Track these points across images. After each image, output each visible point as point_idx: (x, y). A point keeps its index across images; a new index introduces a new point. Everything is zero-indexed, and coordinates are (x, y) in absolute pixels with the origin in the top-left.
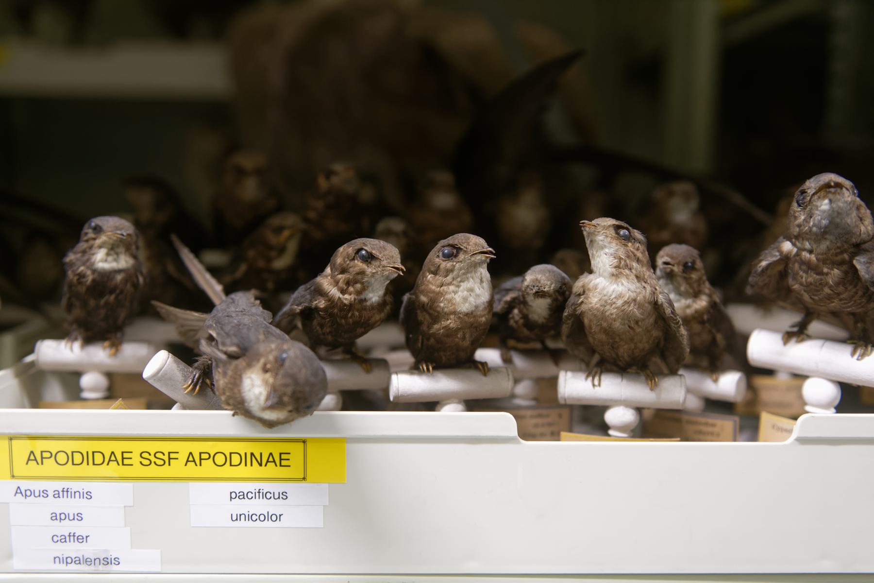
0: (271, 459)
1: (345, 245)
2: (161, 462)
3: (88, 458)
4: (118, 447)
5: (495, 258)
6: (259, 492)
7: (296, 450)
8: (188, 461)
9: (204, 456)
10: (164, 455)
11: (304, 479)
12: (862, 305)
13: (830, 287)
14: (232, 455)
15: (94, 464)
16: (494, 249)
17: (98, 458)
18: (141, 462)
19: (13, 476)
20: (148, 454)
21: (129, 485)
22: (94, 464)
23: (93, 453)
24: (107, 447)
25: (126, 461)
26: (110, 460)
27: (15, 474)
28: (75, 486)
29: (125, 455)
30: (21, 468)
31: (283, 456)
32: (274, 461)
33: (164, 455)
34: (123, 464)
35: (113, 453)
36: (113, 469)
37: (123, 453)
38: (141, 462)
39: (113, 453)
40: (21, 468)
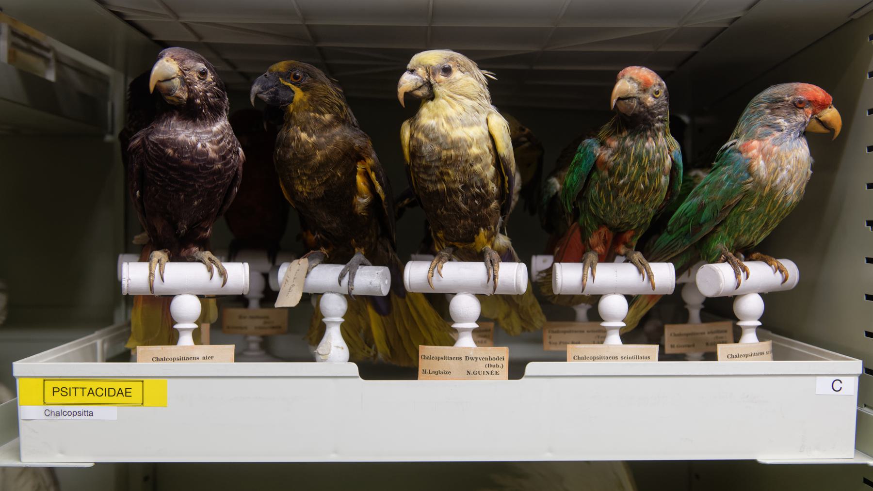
0: (120, 392)
1: (184, 49)
2: (65, 394)
3: (107, 392)
4: (123, 385)
5: (402, 107)
6: (85, 412)
7: (136, 387)
8: (89, 393)
9: (56, 390)
10: (67, 389)
11: (142, 404)
12: (149, 161)
13: (339, 135)
14: (110, 389)
15: (109, 396)
16: (837, 138)
17: (112, 392)
18: (61, 394)
19: (142, 404)
20: (65, 389)
21: (115, 408)
22: (109, 396)
23: (109, 389)
24: (117, 385)
25: (128, 394)
26: (118, 393)
27: (141, 403)
28: (67, 408)
29: (128, 390)
30: (49, 398)
31: (128, 390)
32: (122, 393)
33: (67, 389)
34: (126, 396)
35: (120, 389)
36: (120, 399)
37: (126, 389)
38: (61, 394)
39: (120, 389)
40: (49, 398)
